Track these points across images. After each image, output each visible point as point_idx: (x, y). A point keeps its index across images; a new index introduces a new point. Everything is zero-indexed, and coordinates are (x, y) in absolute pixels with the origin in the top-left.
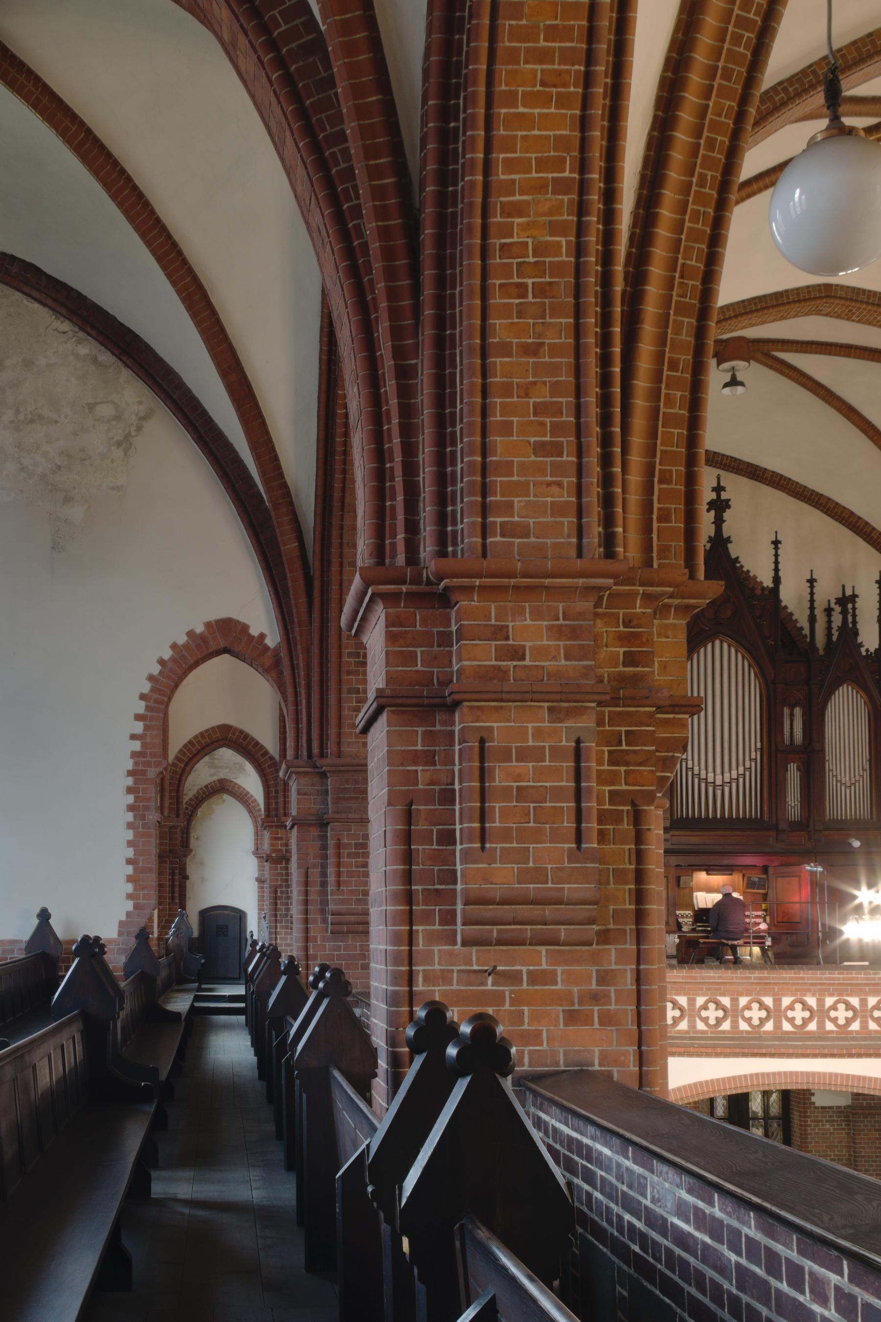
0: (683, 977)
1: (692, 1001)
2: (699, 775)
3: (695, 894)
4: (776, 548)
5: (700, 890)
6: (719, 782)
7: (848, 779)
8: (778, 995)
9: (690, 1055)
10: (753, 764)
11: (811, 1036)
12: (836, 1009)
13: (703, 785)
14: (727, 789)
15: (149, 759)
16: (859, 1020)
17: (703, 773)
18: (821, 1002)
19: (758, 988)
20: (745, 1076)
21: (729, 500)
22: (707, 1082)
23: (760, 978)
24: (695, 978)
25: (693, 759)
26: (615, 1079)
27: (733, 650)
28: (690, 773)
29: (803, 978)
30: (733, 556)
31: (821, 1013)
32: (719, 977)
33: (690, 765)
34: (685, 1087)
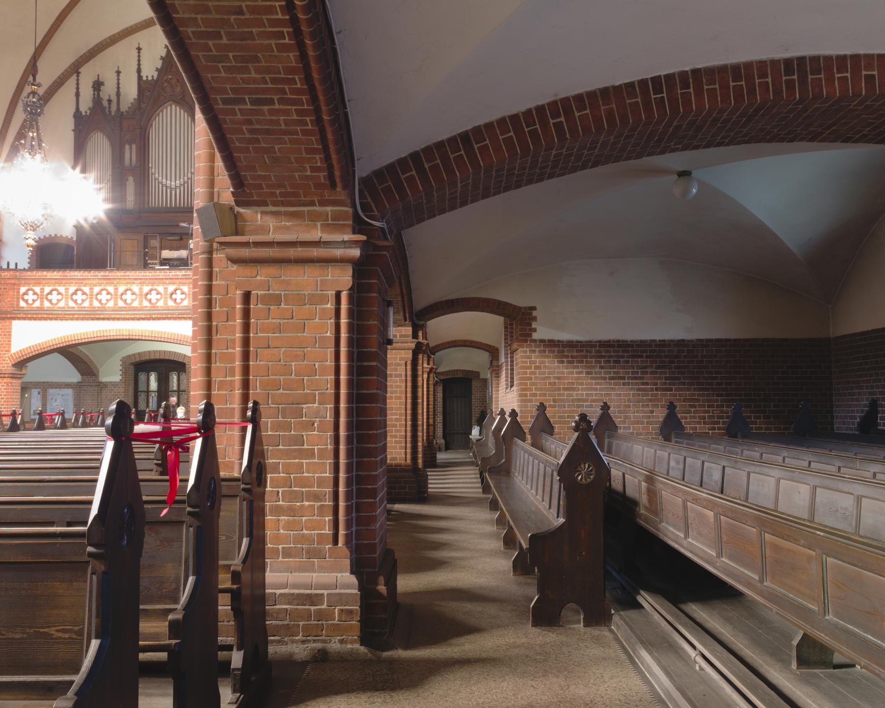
0: (60, 276)
2: (162, 182)
6: (173, 186)
11: (135, 309)
13: (164, 188)
14: (178, 191)
15: (673, 370)
17: (160, 178)
19: (105, 282)
23: (104, 276)
24: (66, 276)
26: (205, 401)
27: (182, 111)
28: (157, 181)
29: (128, 276)
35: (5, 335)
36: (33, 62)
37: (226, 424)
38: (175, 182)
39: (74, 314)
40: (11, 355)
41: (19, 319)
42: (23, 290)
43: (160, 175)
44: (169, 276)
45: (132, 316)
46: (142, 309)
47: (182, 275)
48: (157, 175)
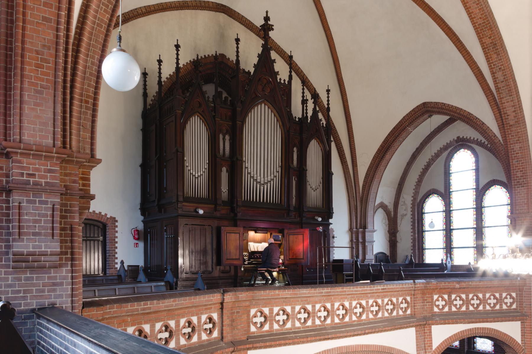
0: (291, 294)
3: (249, 243)
4: (328, 94)
5: (251, 241)
8: (333, 302)
9: (294, 344)
10: (206, 170)
14: (266, 186)
16: (448, 306)
17: (194, 173)
18: (484, 296)
19: (325, 298)
23: (327, 292)
25: (250, 168)
31: (467, 302)
32: (309, 293)
36: (142, 83)
38: (198, 173)
43: (194, 170)
48: (191, 171)
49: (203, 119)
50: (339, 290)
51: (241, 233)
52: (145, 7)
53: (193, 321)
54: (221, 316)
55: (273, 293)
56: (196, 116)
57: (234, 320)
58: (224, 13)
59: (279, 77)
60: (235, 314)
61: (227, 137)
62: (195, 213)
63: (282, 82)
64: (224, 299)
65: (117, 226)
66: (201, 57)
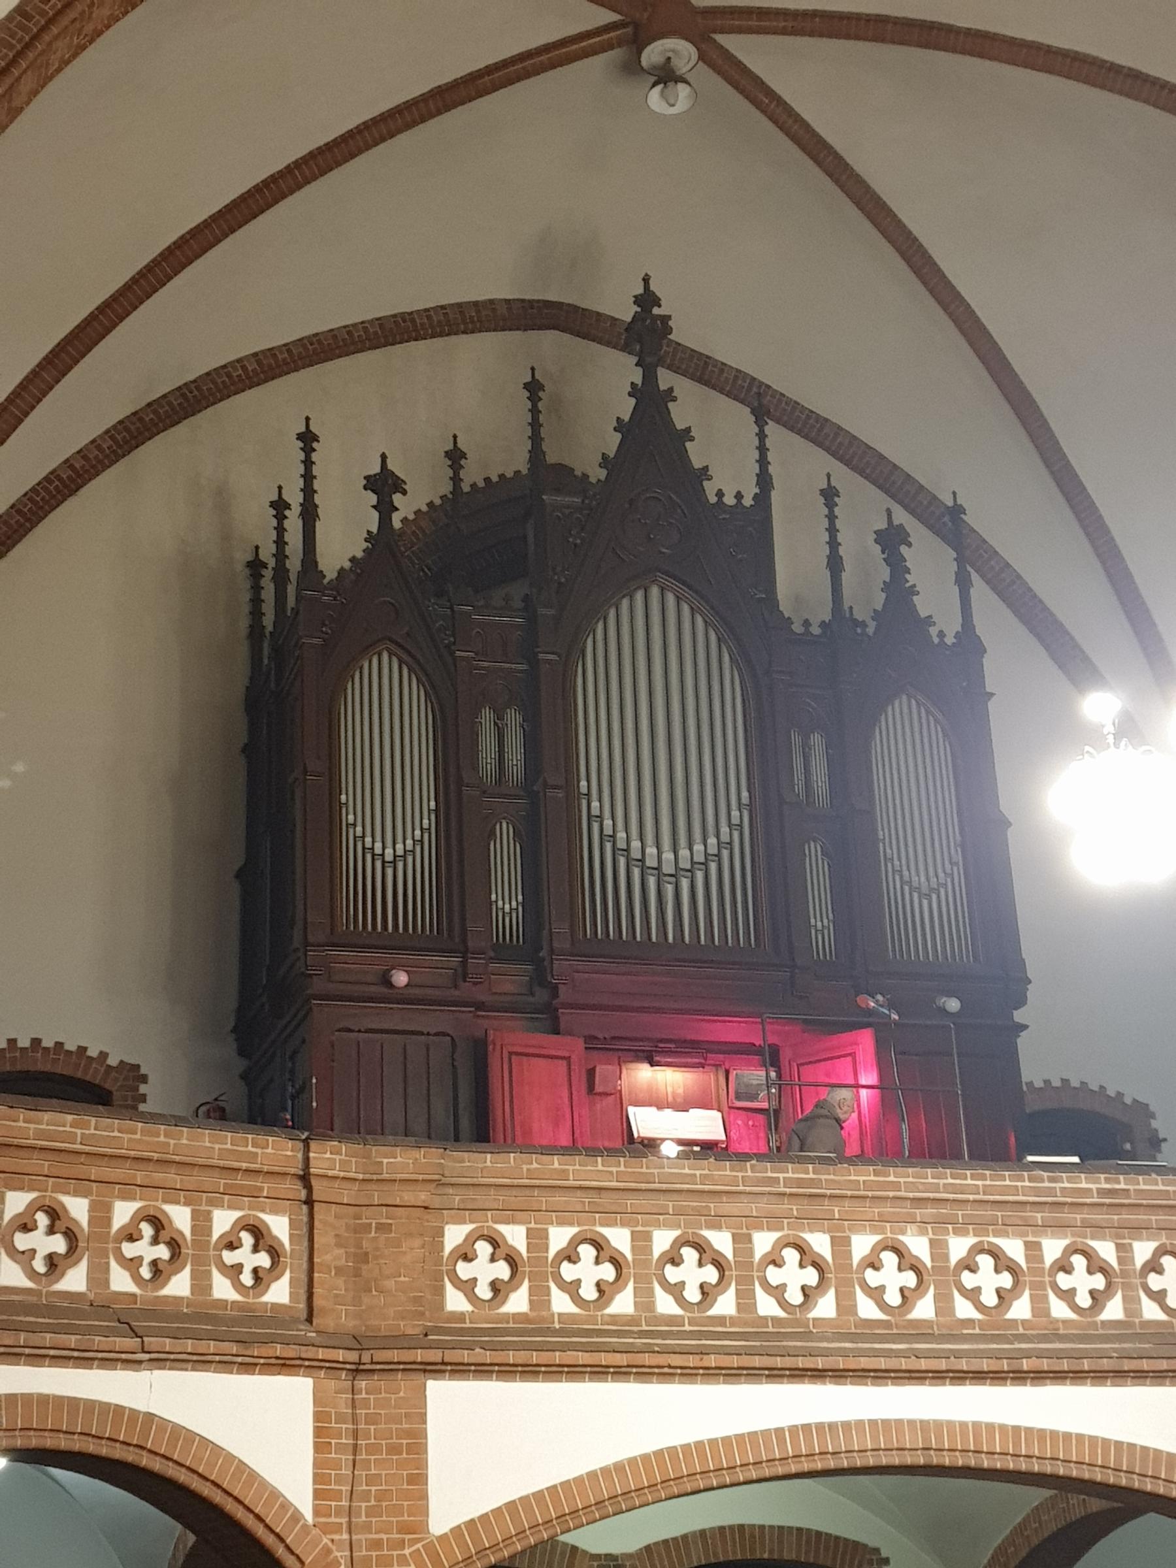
0: (619, 1177)
1: (641, 1241)
5: (638, 1103)
7: (923, 879)
10: (736, 834)
11: (922, 1331)
12: (973, 1269)
14: (685, 884)
16: (1027, 1294)
17: (636, 844)
20: (779, 1431)
21: (669, 317)
22: (686, 1447)
23: (800, 1183)
28: (608, 846)
29: (896, 1186)
30: (680, 425)
33: (608, 830)
34: (632, 1461)
35: (394, 1449)
37: (97, 1351)
38: (691, 849)
39: (702, 1352)
40: (430, 1547)
41: (459, 1370)
42: (454, 1235)
44: (1051, 1192)
45: (942, 1365)
46: (1054, 1331)
47: (1102, 1193)
48: (368, 840)
49: (409, 660)
50: (862, 1178)
51: (574, 1058)
52: (255, 355)
53: (170, 1222)
54: (308, 1232)
55: (535, 1165)
56: (385, 656)
57: (366, 1254)
58: (554, 328)
59: (710, 489)
60: (373, 1234)
61: (513, 718)
62: (384, 990)
63: (729, 500)
64: (307, 1160)
65: (144, 1095)
66: (474, 486)
